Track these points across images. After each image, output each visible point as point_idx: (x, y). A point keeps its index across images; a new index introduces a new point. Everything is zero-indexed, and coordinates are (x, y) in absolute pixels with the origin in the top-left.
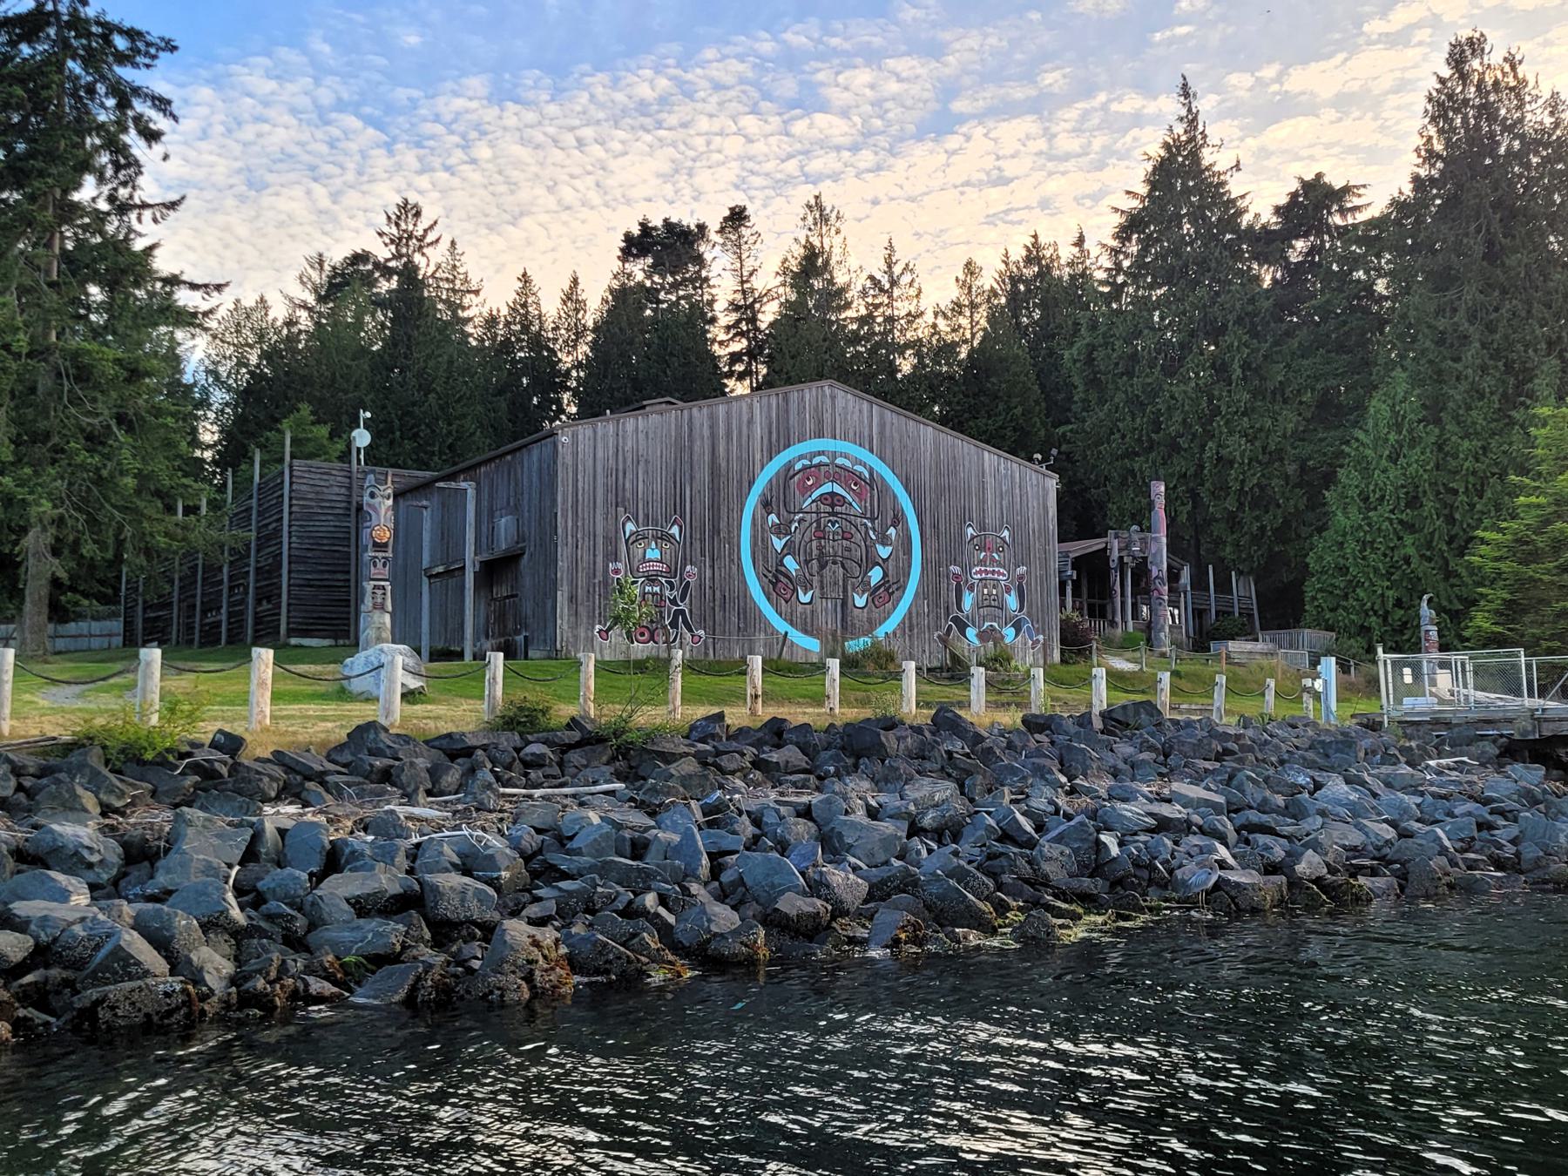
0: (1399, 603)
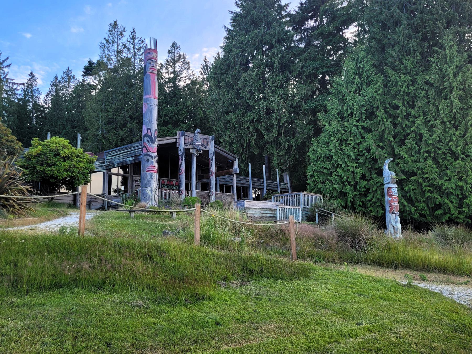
0: (363, 177)
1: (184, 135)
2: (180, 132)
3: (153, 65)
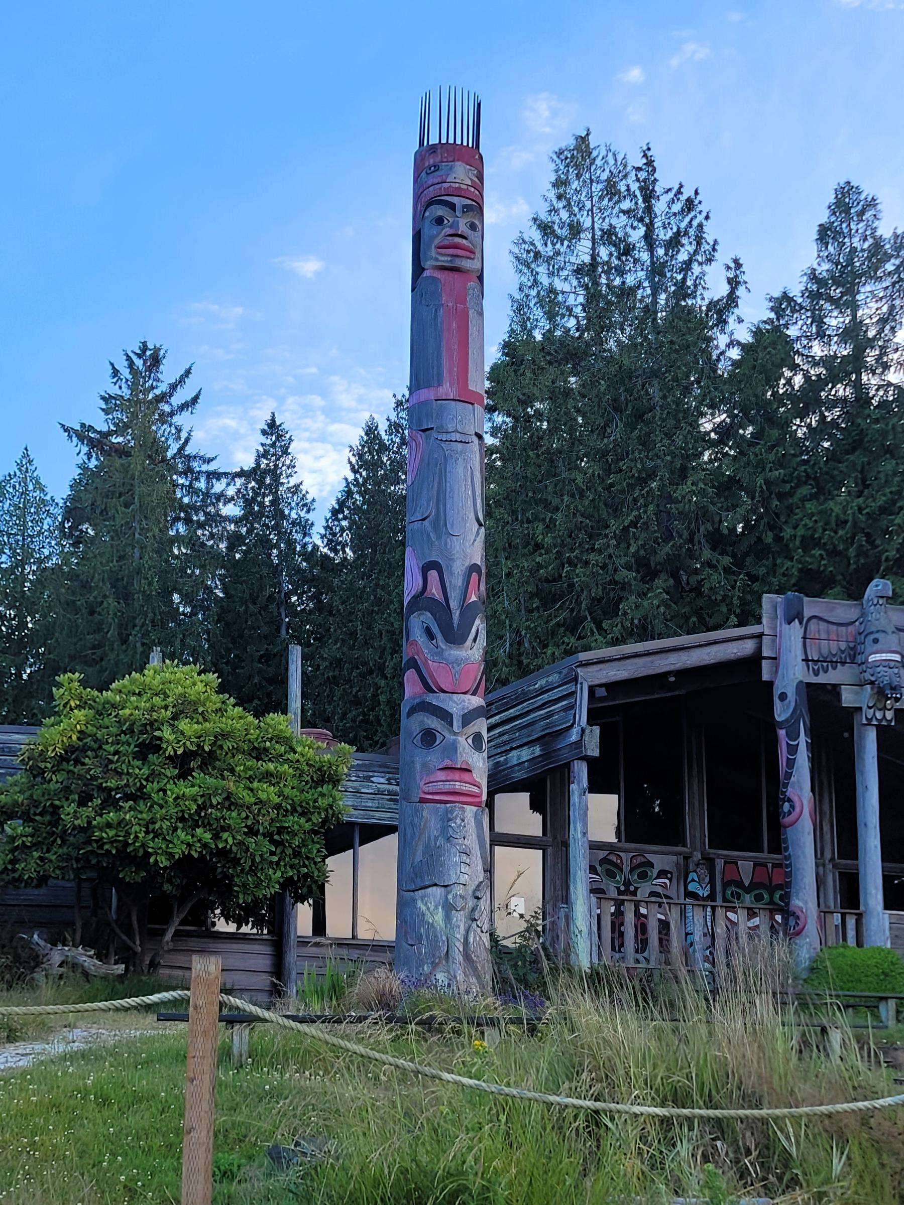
1: (799, 616)
2: (779, 599)
3: (455, 225)
